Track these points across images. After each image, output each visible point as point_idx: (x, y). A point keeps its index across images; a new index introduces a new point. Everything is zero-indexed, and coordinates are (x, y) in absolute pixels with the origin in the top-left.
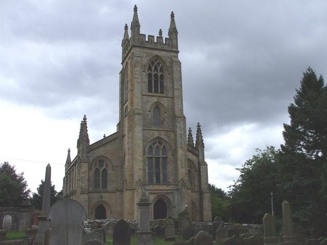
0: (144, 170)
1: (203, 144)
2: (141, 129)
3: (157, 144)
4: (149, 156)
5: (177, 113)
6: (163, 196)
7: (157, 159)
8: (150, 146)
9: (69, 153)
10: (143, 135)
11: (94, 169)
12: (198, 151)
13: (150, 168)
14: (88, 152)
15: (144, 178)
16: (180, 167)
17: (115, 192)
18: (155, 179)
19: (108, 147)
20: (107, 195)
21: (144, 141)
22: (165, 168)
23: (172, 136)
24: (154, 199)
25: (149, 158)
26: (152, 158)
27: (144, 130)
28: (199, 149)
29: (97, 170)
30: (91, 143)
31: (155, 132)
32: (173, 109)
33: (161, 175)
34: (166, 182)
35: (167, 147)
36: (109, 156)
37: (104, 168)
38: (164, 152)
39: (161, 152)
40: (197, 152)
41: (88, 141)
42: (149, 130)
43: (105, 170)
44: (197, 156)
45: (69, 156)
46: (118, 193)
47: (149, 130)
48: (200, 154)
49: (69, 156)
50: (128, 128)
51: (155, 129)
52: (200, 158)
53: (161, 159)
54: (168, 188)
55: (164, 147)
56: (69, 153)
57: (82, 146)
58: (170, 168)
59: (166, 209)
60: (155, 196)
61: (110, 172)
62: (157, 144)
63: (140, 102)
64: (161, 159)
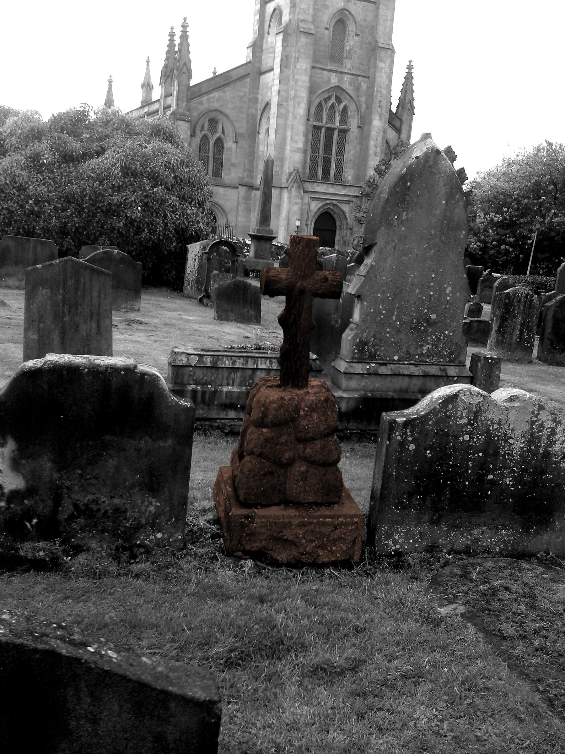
0: (305, 152)
1: (413, 108)
2: (308, 66)
3: (333, 100)
4: (315, 123)
5: (381, 41)
6: (334, 205)
7: (330, 131)
8: (320, 104)
9: (110, 85)
10: (311, 77)
11: (199, 136)
12: (401, 120)
13: (315, 149)
14: (189, 100)
15: (304, 167)
16: (371, 152)
17: (237, 188)
18: (320, 171)
19: (229, 93)
20: (221, 190)
21: (312, 91)
22: (341, 151)
23: (364, 86)
24: (319, 209)
25: (315, 127)
26: (319, 128)
27: (313, 67)
28: (405, 117)
29: (205, 139)
30: (193, 83)
31: (333, 75)
32: (373, 29)
33: (333, 165)
34: (339, 180)
35: (352, 108)
36: (227, 111)
37: (217, 135)
38: (344, 120)
39: (338, 118)
40: (398, 124)
41: (189, 74)
42: (323, 69)
43: (219, 142)
44: (398, 131)
45: (172, 41)
46: (242, 190)
47: (323, 69)
48: (404, 128)
49: (172, 41)
50: (282, 60)
51: (333, 68)
52: (404, 136)
53: (323, 131)
54: (343, 192)
55: (345, 108)
56: (110, 85)
57: (179, 85)
58: (350, 152)
59: (335, 231)
60: (321, 205)
61: (229, 144)
62: (333, 100)
63: (311, 7)
64: (323, 131)
